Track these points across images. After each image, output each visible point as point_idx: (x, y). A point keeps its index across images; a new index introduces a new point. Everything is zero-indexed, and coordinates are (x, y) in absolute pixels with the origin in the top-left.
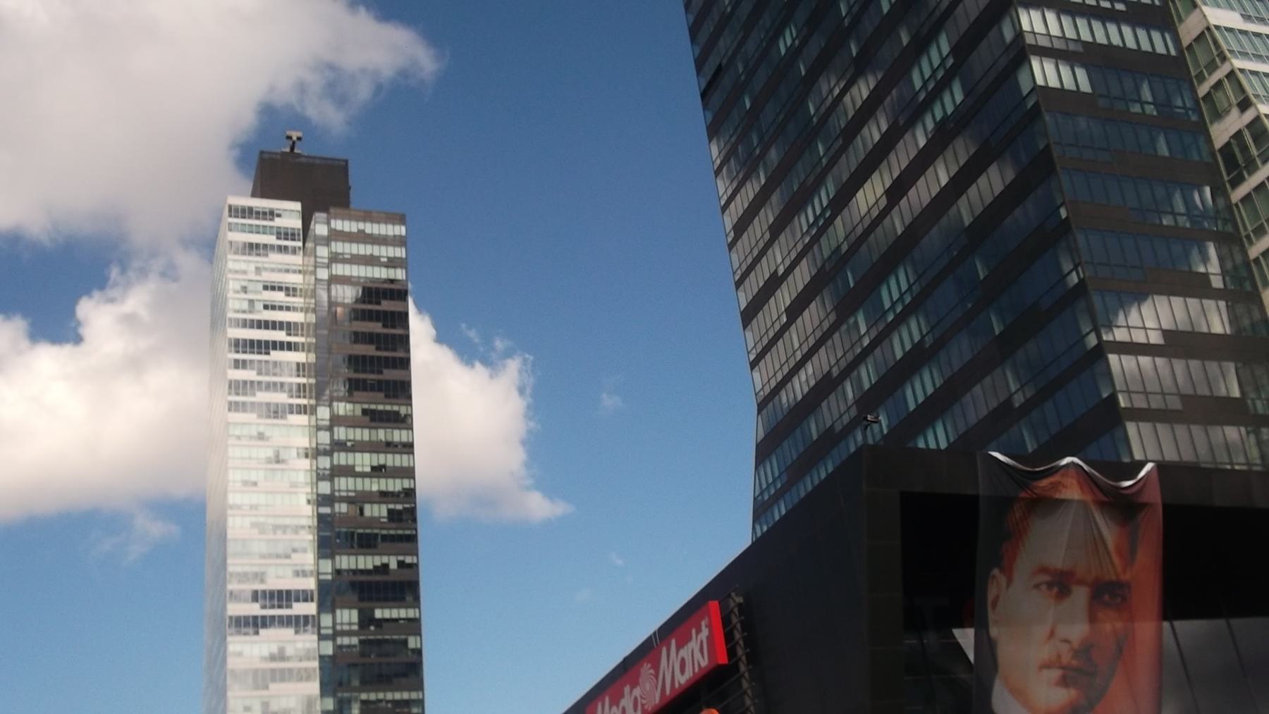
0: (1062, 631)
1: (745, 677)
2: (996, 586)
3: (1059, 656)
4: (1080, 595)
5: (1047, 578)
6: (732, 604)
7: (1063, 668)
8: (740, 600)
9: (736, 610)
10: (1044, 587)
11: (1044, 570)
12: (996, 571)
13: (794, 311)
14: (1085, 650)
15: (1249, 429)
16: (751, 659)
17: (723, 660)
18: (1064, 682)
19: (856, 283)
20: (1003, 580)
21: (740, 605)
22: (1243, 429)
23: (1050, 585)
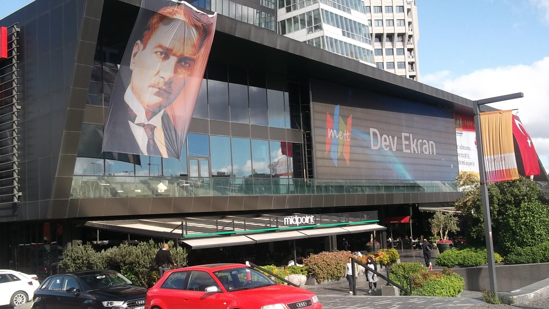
0: (162, 74)
1: (15, 66)
2: (137, 48)
3: (158, 83)
4: (173, 60)
5: (161, 50)
6: (14, 31)
7: (159, 88)
8: (19, 30)
9: (15, 34)
10: (159, 53)
11: (160, 46)
12: (139, 42)
13: (194, 23)
14: (169, 83)
15: (258, 11)
16: (19, 58)
17: (375, 213)
18: (158, 94)
19: (379, 220)
20: (142, 47)
21: (18, 32)
22: (255, 10)
23: (161, 53)
